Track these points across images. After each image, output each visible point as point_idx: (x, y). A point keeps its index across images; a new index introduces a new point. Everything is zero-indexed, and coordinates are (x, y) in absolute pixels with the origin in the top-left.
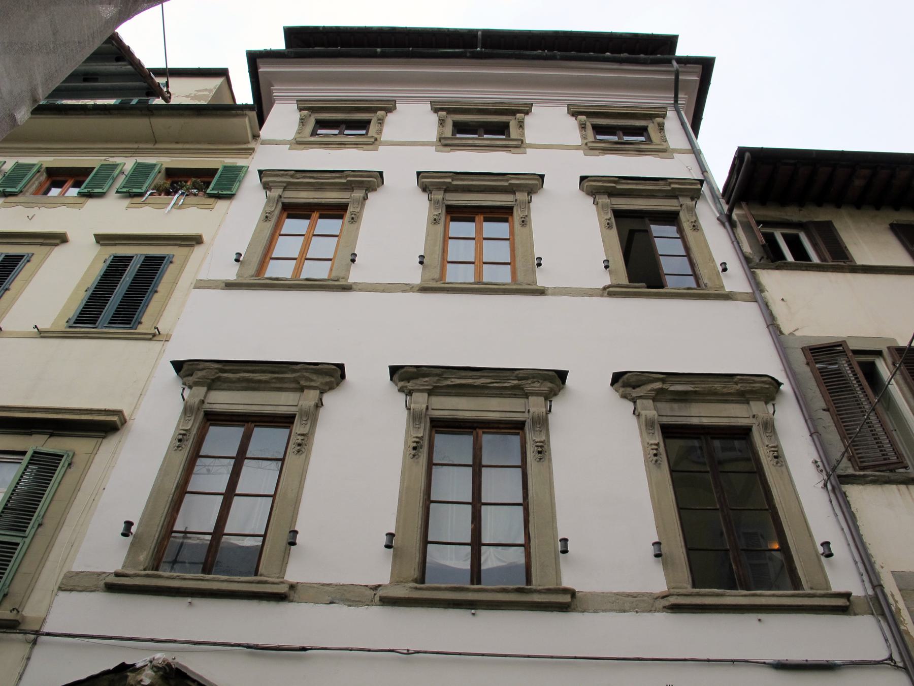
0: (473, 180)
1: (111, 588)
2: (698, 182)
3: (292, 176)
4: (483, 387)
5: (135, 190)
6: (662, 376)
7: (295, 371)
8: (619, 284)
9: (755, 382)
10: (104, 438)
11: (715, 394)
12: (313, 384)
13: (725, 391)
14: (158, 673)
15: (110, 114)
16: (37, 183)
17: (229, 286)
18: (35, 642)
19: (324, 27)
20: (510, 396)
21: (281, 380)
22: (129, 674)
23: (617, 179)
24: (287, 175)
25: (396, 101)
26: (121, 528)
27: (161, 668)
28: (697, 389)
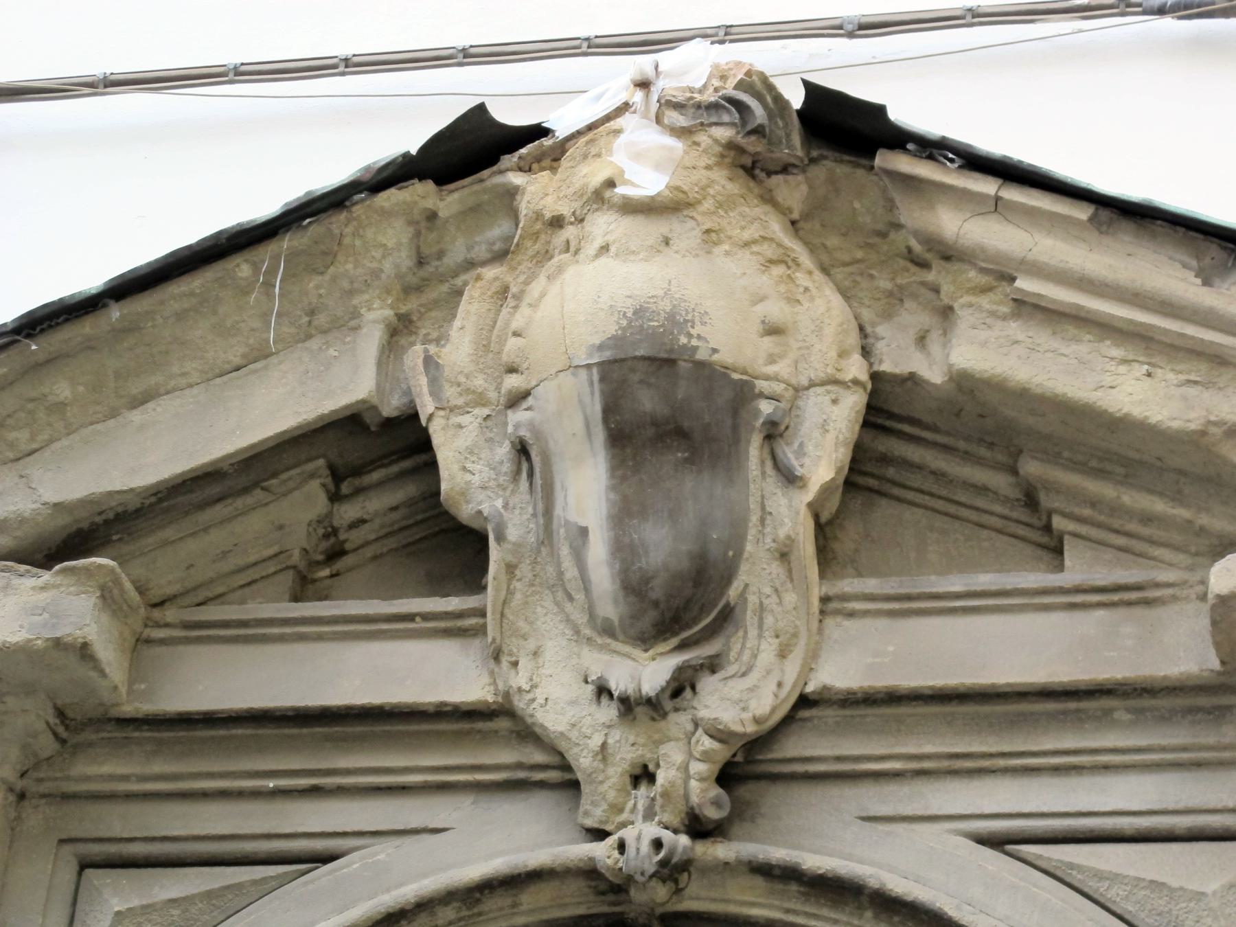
14: (703, 138)
22: (516, 179)
27: (713, 107)
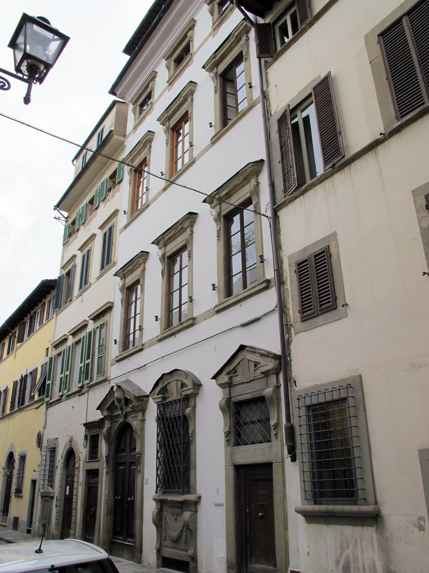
0: (173, 107)
1: (218, 312)
2: (243, 21)
3: (130, 156)
4: (174, 234)
5: (103, 198)
6: (216, 192)
7: (135, 260)
8: (213, 136)
9: (246, 170)
10: (111, 311)
11: (237, 186)
12: (141, 262)
13: (239, 182)
15: (88, 167)
16: (89, 211)
17: (165, 189)
18: (110, 382)
19: (132, 37)
20: (181, 234)
21: (135, 266)
23: (213, 56)
24: (129, 157)
25: (193, 18)
26: (211, 287)
28: (230, 189)
